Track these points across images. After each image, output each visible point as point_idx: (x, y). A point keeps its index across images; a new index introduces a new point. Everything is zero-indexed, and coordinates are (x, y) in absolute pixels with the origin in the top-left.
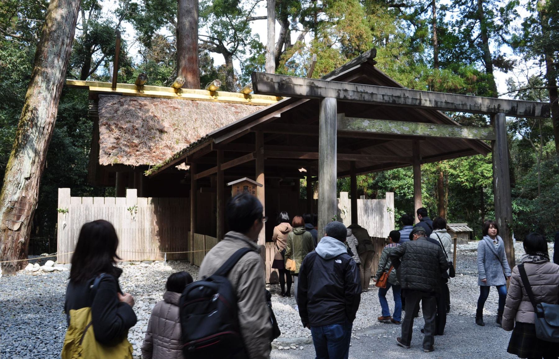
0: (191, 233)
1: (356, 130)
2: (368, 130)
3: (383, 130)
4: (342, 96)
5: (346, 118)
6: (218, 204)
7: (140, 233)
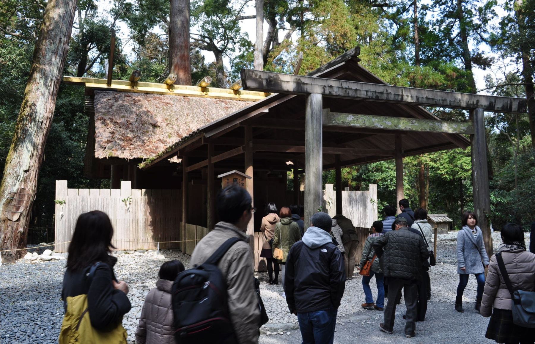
0: (183, 223)
1: (341, 124)
2: (352, 125)
3: (367, 125)
4: (327, 92)
5: (331, 113)
6: (209, 196)
7: (134, 224)
